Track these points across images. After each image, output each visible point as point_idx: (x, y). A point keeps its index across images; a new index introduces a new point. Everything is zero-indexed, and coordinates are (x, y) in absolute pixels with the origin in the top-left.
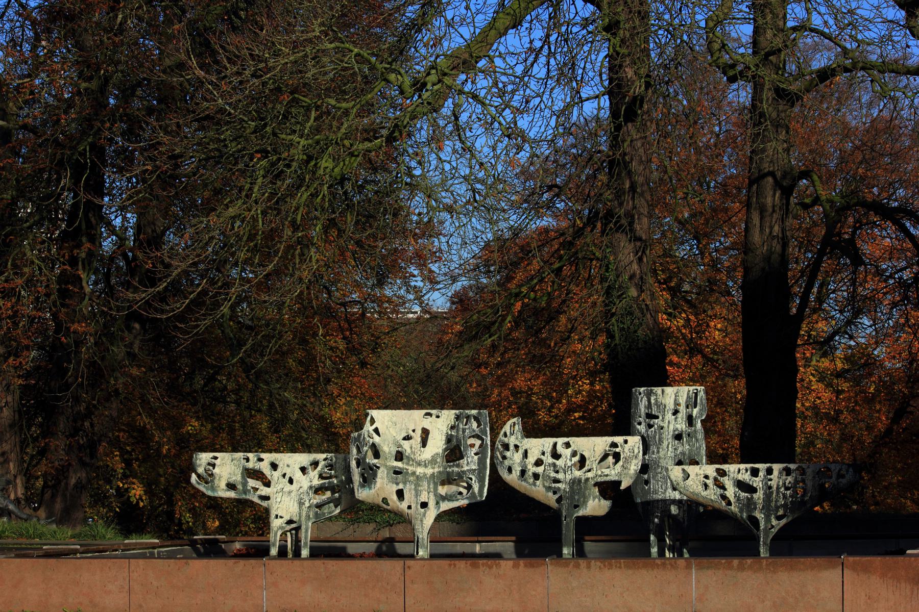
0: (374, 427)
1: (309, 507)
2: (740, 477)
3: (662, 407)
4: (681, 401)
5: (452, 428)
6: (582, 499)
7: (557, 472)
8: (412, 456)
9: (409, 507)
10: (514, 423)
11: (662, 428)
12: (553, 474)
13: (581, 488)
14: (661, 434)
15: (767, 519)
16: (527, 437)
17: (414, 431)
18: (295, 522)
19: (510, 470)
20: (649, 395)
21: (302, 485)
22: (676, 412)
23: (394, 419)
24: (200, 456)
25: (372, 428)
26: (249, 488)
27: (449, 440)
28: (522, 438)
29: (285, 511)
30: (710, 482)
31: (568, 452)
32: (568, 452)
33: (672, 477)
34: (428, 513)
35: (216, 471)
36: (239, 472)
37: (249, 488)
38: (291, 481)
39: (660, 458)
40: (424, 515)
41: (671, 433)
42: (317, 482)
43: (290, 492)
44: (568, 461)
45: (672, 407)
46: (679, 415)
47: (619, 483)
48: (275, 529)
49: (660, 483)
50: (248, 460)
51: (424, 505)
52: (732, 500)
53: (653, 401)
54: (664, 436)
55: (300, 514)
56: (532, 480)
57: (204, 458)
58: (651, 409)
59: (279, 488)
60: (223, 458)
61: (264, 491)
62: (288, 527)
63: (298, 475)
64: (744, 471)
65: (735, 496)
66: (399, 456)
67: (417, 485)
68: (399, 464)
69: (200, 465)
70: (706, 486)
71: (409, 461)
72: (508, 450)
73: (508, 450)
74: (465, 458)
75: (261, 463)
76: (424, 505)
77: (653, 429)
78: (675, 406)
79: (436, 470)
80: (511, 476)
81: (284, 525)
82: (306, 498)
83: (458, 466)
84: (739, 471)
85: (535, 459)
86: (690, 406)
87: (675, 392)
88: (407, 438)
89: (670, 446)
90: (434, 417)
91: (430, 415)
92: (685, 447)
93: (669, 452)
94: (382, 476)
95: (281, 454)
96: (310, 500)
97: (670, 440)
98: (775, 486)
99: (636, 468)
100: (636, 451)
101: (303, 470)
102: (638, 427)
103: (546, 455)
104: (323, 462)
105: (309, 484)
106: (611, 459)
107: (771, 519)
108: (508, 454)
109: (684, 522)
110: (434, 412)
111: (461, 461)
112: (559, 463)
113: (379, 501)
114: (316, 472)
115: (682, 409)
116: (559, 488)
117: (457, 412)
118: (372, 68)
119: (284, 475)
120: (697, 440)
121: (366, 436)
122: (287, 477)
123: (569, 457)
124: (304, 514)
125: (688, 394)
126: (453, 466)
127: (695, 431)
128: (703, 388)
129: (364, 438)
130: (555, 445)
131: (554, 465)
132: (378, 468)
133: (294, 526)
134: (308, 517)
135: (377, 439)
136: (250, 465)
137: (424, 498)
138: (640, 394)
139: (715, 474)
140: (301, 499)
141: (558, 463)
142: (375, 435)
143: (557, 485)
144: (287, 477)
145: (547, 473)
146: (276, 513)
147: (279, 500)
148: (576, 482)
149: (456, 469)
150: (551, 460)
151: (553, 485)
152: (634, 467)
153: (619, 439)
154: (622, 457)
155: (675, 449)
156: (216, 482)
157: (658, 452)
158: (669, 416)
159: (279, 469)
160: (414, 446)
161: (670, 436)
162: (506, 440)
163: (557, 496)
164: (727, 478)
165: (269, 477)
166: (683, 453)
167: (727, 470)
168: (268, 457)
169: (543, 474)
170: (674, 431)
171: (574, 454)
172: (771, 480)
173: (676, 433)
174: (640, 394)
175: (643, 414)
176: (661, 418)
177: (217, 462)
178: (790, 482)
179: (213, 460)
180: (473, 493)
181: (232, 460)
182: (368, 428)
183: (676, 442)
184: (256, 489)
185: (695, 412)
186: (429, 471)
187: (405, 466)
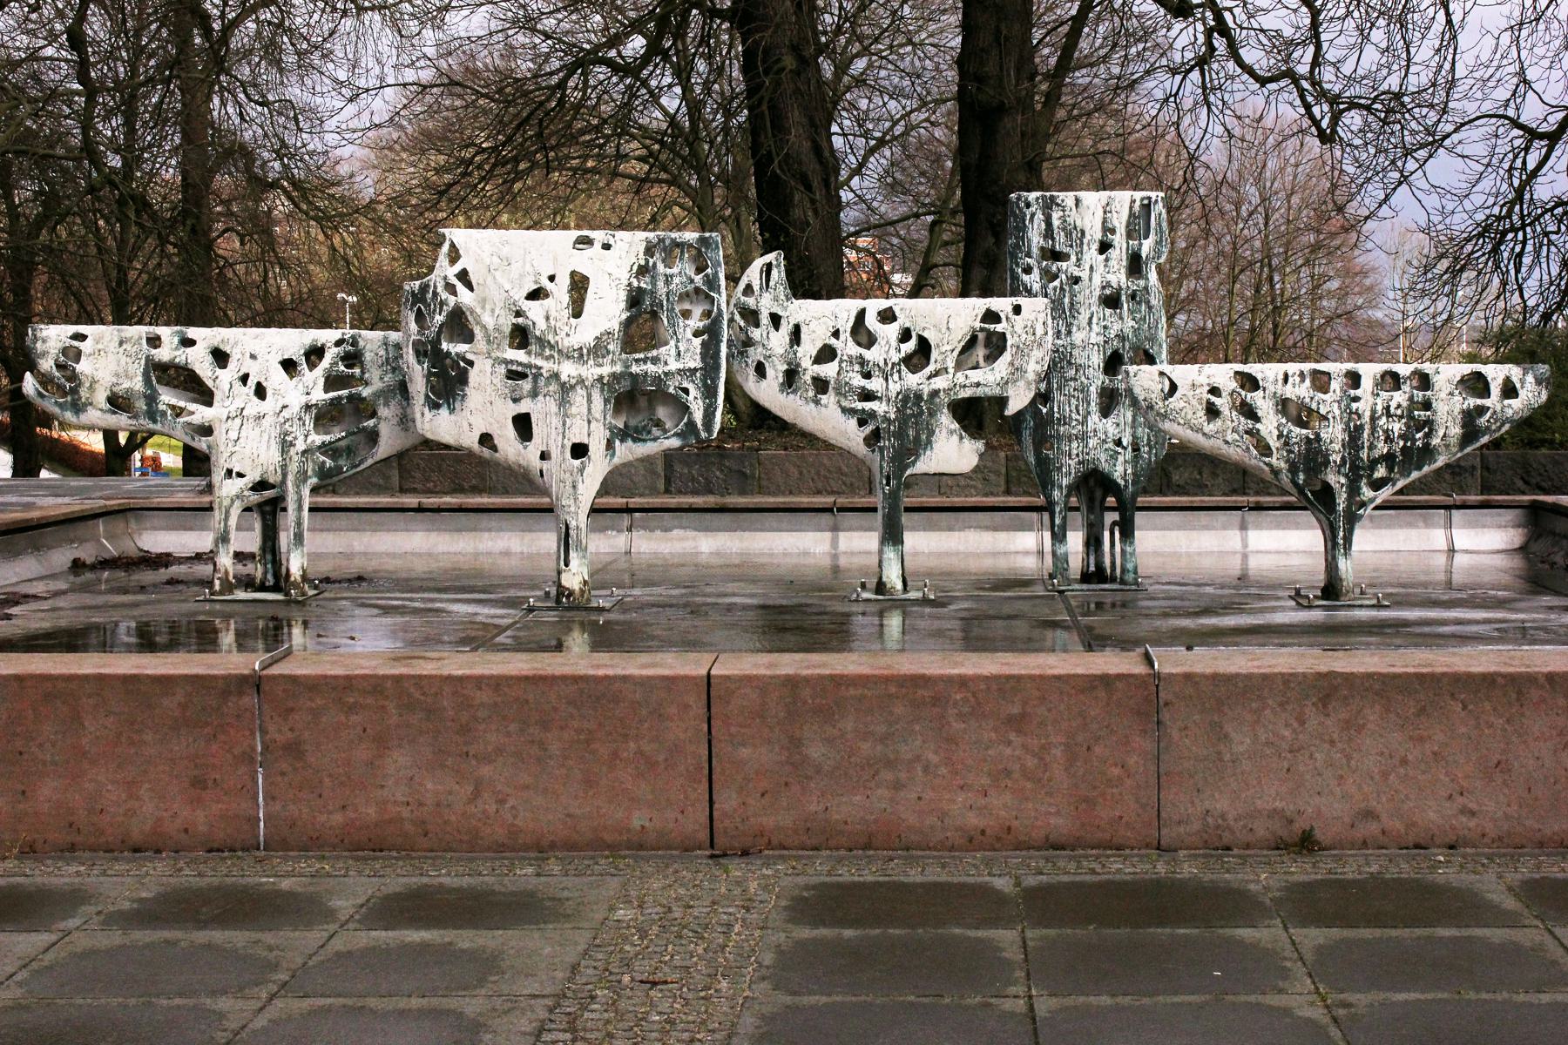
0: (458, 268)
1: (304, 452)
2: (1290, 392)
3: (1076, 236)
5: (643, 270)
7: (867, 376)
8: (550, 338)
9: (544, 456)
10: (769, 266)
11: (1077, 280)
12: (858, 381)
13: (922, 412)
14: (1073, 296)
15: (1353, 490)
16: (796, 296)
17: (552, 278)
18: (273, 487)
19: (760, 370)
20: (1049, 205)
21: (286, 402)
22: (1104, 247)
24: (45, 333)
25: (451, 272)
26: (162, 407)
27: (635, 299)
29: (248, 462)
30: (1222, 403)
31: (891, 331)
32: (891, 331)
33: (1137, 390)
35: (83, 367)
36: (138, 369)
37: (162, 407)
38: (260, 392)
40: (582, 470)
41: (1097, 293)
42: (319, 395)
44: (893, 352)
45: (1098, 236)
46: (1114, 253)
47: (1002, 401)
48: (226, 503)
49: (1073, 401)
50: (154, 341)
51: (580, 451)
52: (1274, 443)
53: (1056, 223)
54: (1080, 298)
55: (284, 468)
57: (52, 337)
58: (1053, 239)
59: (233, 408)
60: (100, 336)
61: (200, 414)
62: (255, 498)
63: (277, 379)
64: (1298, 379)
65: (1280, 436)
66: (521, 336)
67: (564, 402)
68: (520, 356)
69: (44, 354)
70: (1212, 412)
71: (543, 347)
73: (757, 325)
74: (672, 343)
75: (189, 350)
76: (580, 451)
77: (1057, 283)
79: (606, 370)
80: (764, 383)
81: (246, 493)
82: (297, 431)
83: (655, 360)
85: (819, 345)
86: (1135, 235)
87: (1104, 202)
88: (536, 295)
89: (1095, 320)
90: (597, 246)
91: (588, 241)
92: (1123, 323)
94: (484, 379)
95: (234, 330)
98: (1368, 414)
99: (1038, 368)
100: (1040, 331)
101: (289, 366)
102: (1025, 278)
103: (842, 337)
104: (336, 350)
105: (304, 399)
106: (980, 352)
107: (1359, 488)
108: (756, 334)
109: (1126, 487)
110: (599, 236)
111: (663, 350)
112: (873, 355)
113: (471, 441)
114: (319, 371)
115: (1119, 239)
116: (872, 414)
117: (651, 235)
118: (79, 167)
119: (244, 379)
121: (439, 290)
122: (252, 382)
123: (894, 343)
124: (293, 468)
125: (1131, 208)
126: (645, 361)
127: (1146, 288)
128: (1162, 194)
129: (435, 294)
130: (861, 315)
131: (862, 361)
132: (471, 363)
134: (302, 477)
135: (464, 296)
136: (164, 354)
137: (577, 435)
138: (1028, 205)
139: (1234, 385)
140: (286, 434)
142: (460, 287)
143: (868, 406)
144: (252, 382)
145: (846, 377)
146: (227, 466)
147: (233, 435)
148: (910, 399)
149: (650, 368)
150: (853, 349)
151: (859, 405)
152: (1035, 364)
153: (1002, 304)
154: (1009, 343)
156: (84, 393)
157: (1069, 333)
158: (1091, 254)
159: (232, 365)
160: (553, 314)
161: (1095, 299)
162: (750, 302)
163: (869, 429)
164: (1260, 393)
165: (210, 383)
166: (1121, 337)
167: (1259, 377)
168: (205, 336)
169: (837, 380)
170: (1103, 288)
171: (905, 336)
172: (1356, 399)
173: (1108, 292)
174: (1028, 205)
175: (1035, 251)
176: (1073, 258)
177: (85, 346)
178: (1399, 406)
179: (76, 343)
180: (691, 424)
181: (121, 343)
182: (444, 270)
183: (1108, 312)
184: (178, 412)
185: (1147, 246)
187: (539, 362)
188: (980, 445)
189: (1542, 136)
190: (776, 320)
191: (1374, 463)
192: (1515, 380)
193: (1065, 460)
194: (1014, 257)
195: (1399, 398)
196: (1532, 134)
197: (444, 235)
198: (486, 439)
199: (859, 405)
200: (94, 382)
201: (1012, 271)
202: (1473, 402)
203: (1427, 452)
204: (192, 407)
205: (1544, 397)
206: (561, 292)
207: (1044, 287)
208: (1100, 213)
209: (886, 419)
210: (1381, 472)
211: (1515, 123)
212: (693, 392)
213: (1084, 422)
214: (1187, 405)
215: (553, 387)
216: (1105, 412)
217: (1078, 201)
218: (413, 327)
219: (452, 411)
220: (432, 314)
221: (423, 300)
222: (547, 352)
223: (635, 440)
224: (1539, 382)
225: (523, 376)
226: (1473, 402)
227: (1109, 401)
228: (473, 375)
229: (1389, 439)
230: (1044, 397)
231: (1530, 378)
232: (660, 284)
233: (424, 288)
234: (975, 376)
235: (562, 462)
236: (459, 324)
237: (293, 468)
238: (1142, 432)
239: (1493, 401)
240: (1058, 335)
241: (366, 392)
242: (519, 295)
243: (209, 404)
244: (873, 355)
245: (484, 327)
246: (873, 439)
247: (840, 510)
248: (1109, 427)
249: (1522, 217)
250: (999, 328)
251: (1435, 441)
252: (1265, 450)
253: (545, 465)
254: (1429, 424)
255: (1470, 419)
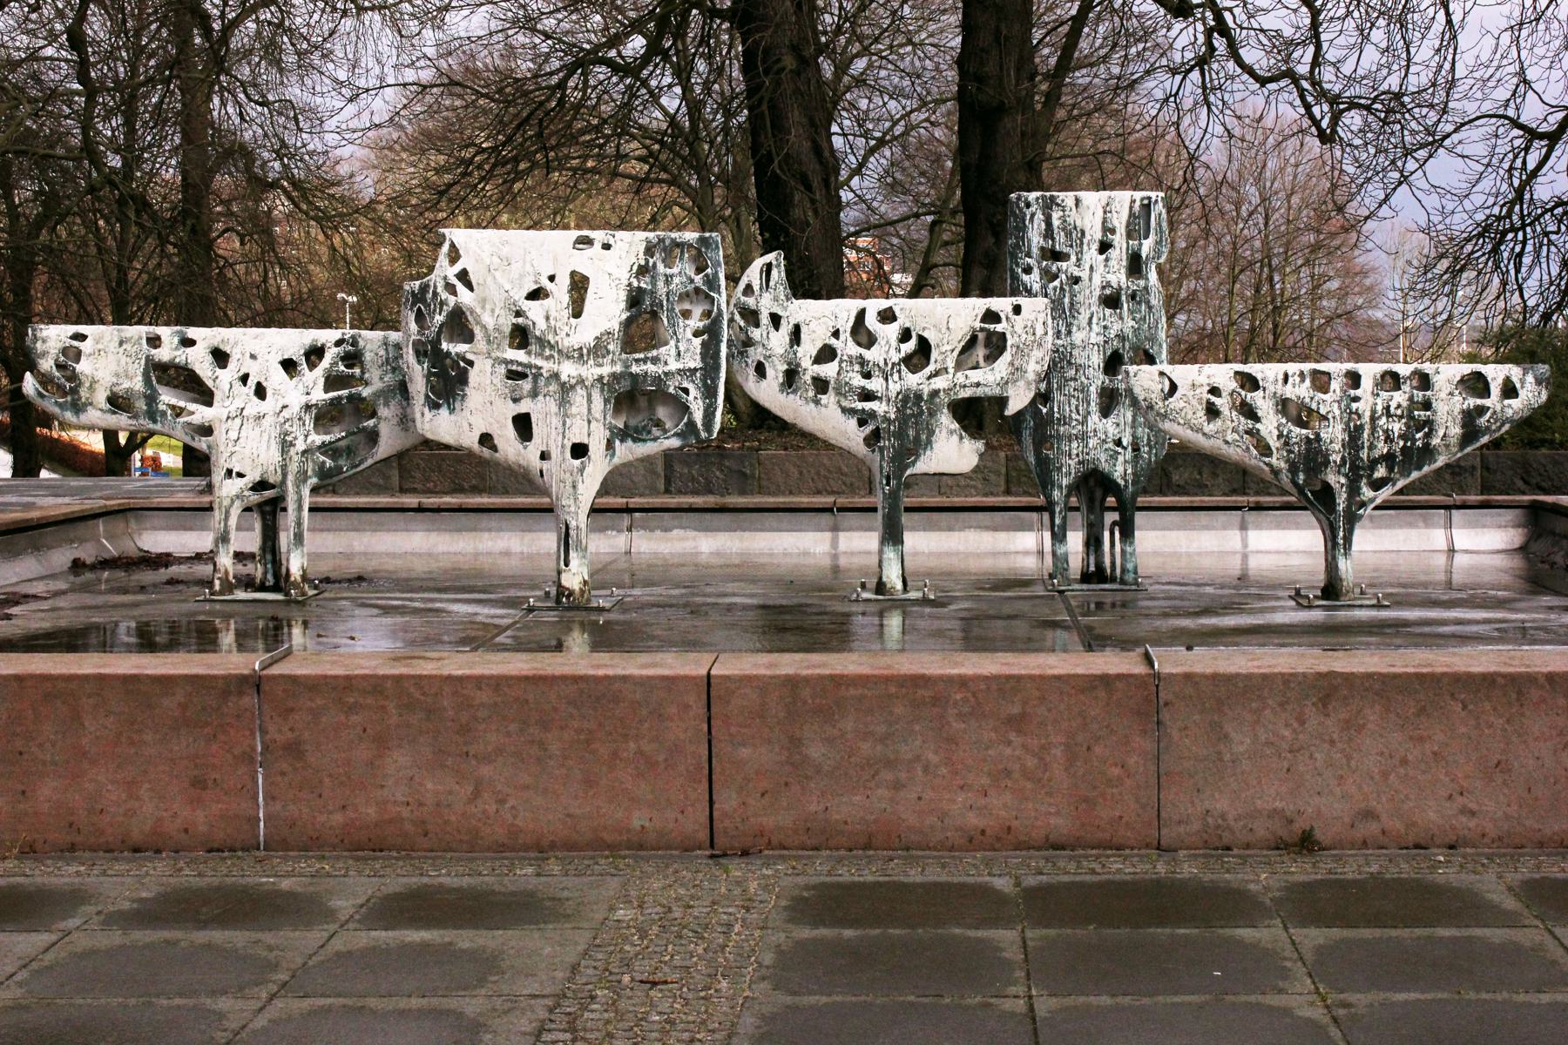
0: (458, 268)
1: (304, 452)
2: (1290, 392)
3: (1076, 236)
4: (1116, 223)
5: (643, 270)
6: (924, 437)
7: (867, 376)
8: (550, 338)
10: (769, 266)
11: (1077, 280)
12: (858, 381)
14: (1073, 296)
15: (1353, 490)
16: (796, 296)
17: (552, 278)
18: (273, 487)
19: (760, 370)
20: (1049, 205)
21: (286, 402)
22: (1104, 247)
23: (505, 251)
24: (44, 334)
25: (451, 272)
26: (162, 407)
27: (635, 299)
28: (788, 299)
29: (248, 462)
30: (1222, 403)
31: (891, 331)
32: (891, 331)
34: (588, 470)
35: (83, 367)
36: (138, 369)
37: (162, 407)
38: (260, 392)
39: (1073, 346)
40: (582, 470)
41: (1097, 293)
42: (319, 395)
43: (259, 418)
44: (893, 352)
45: (1098, 235)
46: (1114, 253)
47: (1002, 401)
48: (226, 503)
49: (1073, 401)
50: (154, 341)
51: (580, 451)
52: (1274, 443)
53: (1056, 223)
54: (1080, 298)
55: (284, 468)
56: (811, 394)
57: (52, 337)
58: (1053, 239)
59: (233, 408)
61: (200, 414)
62: (255, 498)
63: (277, 379)
64: (1298, 379)
65: (1280, 436)
66: (521, 336)
67: (564, 402)
68: (520, 356)
69: (44, 354)
70: (1212, 412)
71: (543, 347)
72: (757, 325)
73: (757, 325)
74: (672, 343)
75: (189, 350)
76: (580, 451)
77: (1057, 283)
78: (1104, 234)
79: (606, 370)
80: (764, 383)
82: (297, 431)
83: (655, 360)
84: (1286, 379)
85: (819, 345)
86: (1135, 235)
87: (1104, 202)
88: (536, 295)
89: (1095, 320)
90: (597, 246)
91: (588, 242)
92: (1123, 323)
93: (1093, 335)
94: (484, 378)
95: (234, 330)
96: (306, 436)
97: (1094, 308)
98: (1368, 414)
99: (1038, 368)
100: (1040, 331)
101: (289, 366)
102: (1025, 278)
103: (842, 337)
104: (336, 350)
105: (304, 399)
106: (980, 352)
108: (756, 334)
109: (1126, 487)
110: (599, 236)
111: (663, 350)
112: (873, 355)
113: (471, 440)
114: (320, 371)
115: (1119, 239)
116: (872, 414)
117: (651, 235)
119: (244, 379)
120: (1150, 308)
123: (894, 343)
124: (293, 468)
125: (1131, 208)
126: (645, 361)
127: (1146, 288)
128: (1162, 194)
129: (435, 294)
130: (861, 315)
131: (862, 361)
132: (471, 363)
133: (269, 494)
134: (302, 477)
135: (464, 296)
136: (164, 354)
137: (577, 435)
138: (1028, 205)
139: (1234, 385)
140: (286, 434)
141: (869, 355)
142: (460, 287)
143: (868, 406)
144: (252, 382)
145: (845, 377)
146: (227, 466)
147: (233, 435)
148: (910, 399)
149: (650, 368)
150: (853, 349)
151: (860, 405)
152: (1035, 364)
153: (1002, 304)
154: (1009, 343)
155: (1105, 327)
156: (84, 393)
157: (1069, 333)
158: (1091, 254)
159: (232, 365)
160: (553, 314)
161: (1095, 299)
162: (750, 302)
163: (869, 429)
164: (1260, 393)
165: (210, 383)
166: (1121, 337)
167: (1259, 377)
168: (204, 336)
170: (1103, 288)
171: (905, 336)
172: (1356, 399)
173: (1108, 292)
174: (1028, 205)
175: (1035, 251)
176: (1073, 258)
177: (85, 346)
178: (1399, 406)
179: (75, 343)
180: (691, 424)
181: (121, 344)
182: (444, 270)
183: (1108, 311)
184: (178, 412)
185: (1147, 246)
186: (591, 371)
187: (539, 362)
188: (980, 445)
189: (1542, 136)
190: (776, 320)
191: (1374, 463)
192: (1515, 380)
193: (1065, 460)
194: (1014, 257)
195: (1399, 398)
196: (1532, 134)
197: (444, 236)
198: (486, 439)
199: (860, 405)
200: (94, 382)
201: (1012, 270)
202: (1473, 402)
203: (1428, 452)
204: (192, 407)
205: (1544, 396)
206: (561, 292)
207: (1044, 287)
208: (1100, 213)
209: (886, 419)
210: (1381, 472)
211: (1515, 123)
212: (693, 392)
213: (1084, 422)
214: (1187, 405)
215: (553, 387)
216: (1105, 412)
217: (1078, 201)
218: (413, 327)
219: (452, 411)
220: (432, 314)
221: (423, 300)
222: (547, 352)
223: (635, 440)
224: (1539, 382)
225: (523, 376)
226: (1473, 402)
227: (1109, 401)
228: (473, 375)
229: (1389, 439)
230: (1044, 397)
231: (1530, 378)
232: (660, 284)
233: (424, 288)
234: (975, 376)
235: (562, 462)
236: (459, 324)
237: (293, 468)
238: (1143, 432)
239: (1493, 401)
240: (1058, 335)
241: (366, 392)
242: (519, 295)
243: (209, 403)
244: (873, 355)
245: (484, 327)
246: (873, 439)
247: (840, 510)
248: (1109, 427)
249: (1522, 217)
250: (999, 328)
251: (1435, 441)
252: (1265, 450)
253: (545, 465)
254: (1429, 424)
255: (1470, 419)
